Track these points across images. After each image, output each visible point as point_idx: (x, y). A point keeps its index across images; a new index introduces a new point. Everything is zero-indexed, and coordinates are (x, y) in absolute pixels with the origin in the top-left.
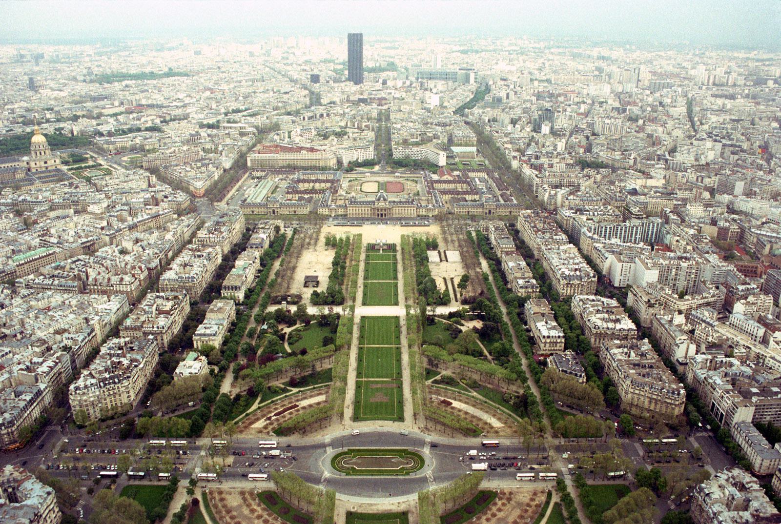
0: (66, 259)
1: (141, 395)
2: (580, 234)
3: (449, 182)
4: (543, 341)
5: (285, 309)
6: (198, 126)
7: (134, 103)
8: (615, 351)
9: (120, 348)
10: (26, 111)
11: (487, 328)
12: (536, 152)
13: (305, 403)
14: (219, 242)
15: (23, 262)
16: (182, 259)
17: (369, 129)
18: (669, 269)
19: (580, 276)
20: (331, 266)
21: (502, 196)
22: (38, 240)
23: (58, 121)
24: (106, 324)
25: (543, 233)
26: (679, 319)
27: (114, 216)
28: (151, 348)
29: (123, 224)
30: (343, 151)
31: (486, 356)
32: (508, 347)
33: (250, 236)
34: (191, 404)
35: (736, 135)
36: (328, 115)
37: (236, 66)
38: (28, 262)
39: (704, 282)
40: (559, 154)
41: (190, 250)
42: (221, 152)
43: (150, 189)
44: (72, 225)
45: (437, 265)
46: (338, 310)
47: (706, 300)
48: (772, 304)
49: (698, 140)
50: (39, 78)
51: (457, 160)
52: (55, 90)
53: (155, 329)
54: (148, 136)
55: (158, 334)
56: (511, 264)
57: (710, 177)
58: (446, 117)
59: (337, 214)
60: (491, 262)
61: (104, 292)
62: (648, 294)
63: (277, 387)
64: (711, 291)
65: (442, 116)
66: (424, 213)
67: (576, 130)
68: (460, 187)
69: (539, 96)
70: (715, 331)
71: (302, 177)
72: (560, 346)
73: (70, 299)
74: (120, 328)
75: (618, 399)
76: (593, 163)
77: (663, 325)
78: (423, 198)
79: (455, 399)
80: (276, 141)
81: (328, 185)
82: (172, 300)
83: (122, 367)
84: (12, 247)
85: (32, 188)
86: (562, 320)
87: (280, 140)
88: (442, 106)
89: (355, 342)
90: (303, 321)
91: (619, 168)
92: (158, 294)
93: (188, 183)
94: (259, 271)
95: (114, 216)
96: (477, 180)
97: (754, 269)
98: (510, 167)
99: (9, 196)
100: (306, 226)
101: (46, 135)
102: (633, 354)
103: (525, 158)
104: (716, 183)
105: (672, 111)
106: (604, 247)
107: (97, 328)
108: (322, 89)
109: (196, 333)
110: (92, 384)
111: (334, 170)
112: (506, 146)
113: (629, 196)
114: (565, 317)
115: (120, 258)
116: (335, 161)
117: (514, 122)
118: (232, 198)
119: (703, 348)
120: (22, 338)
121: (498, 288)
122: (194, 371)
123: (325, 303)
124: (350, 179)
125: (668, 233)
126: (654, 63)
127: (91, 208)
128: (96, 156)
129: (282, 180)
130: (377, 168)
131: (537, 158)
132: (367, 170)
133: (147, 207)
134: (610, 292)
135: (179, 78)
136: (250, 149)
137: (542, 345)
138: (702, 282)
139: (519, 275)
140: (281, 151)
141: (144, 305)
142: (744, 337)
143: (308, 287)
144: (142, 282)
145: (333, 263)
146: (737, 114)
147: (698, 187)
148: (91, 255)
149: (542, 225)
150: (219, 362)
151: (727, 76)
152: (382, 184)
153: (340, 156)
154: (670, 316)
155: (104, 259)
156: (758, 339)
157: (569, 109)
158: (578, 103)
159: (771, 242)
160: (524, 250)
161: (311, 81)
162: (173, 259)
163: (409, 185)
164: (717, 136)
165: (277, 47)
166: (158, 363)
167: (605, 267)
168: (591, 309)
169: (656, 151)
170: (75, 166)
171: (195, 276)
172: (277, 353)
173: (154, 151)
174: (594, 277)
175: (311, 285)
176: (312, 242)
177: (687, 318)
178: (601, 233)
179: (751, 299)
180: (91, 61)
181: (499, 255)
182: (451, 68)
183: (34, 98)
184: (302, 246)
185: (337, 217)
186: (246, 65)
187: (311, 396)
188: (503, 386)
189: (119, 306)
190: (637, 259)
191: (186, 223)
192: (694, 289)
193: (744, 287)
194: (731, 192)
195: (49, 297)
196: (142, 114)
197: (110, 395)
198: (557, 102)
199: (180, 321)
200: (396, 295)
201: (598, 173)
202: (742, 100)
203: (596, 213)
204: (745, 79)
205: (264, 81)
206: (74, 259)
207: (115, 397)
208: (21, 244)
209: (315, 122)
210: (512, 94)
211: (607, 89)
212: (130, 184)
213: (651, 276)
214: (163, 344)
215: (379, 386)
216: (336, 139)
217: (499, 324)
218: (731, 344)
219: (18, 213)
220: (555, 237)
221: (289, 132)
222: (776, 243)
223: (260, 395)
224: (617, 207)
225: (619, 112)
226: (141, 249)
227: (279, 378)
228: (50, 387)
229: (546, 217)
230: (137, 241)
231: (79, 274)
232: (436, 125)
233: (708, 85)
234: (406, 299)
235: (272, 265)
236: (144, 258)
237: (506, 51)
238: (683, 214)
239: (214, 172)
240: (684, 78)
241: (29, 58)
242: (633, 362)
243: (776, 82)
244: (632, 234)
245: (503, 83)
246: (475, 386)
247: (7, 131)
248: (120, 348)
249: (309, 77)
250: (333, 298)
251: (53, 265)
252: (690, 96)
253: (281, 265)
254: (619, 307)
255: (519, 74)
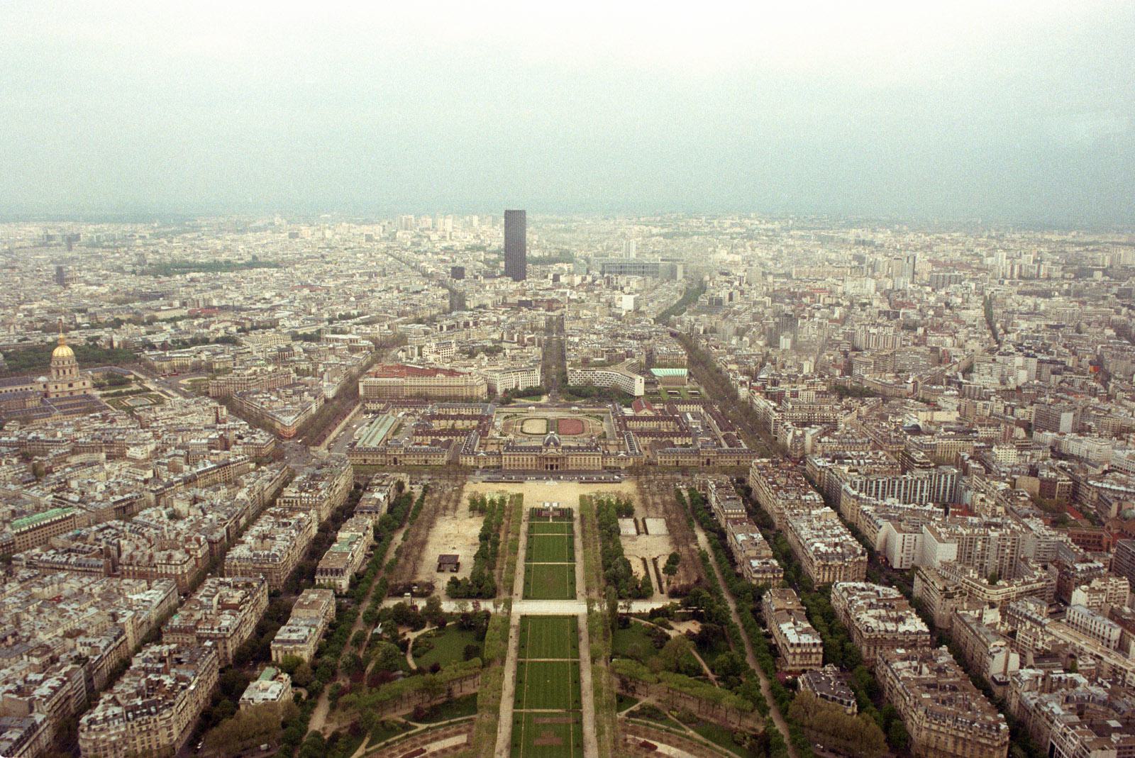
0: (90, 526)
1: (189, 732)
2: (840, 492)
3: (649, 419)
4: (791, 651)
5: (409, 604)
6: (289, 337)
7: (201, 304)
8: (899, 665)
9: (162, 660)
10: (49, 312)
11: (708, 633)
12: (773, 375)
13: (435, 747)
14: (314, 505)
15: (27, 528)
16: (260, 529)
17: (534, 344)
18: (972, 541)
19: (843, 554)
20: (477, 540)
21: (725, 438)
22: (50, 497)
23: (93, 327)
24: (142, 623)
25: (787, 491)
26: (992, 616)
27: (164, 464)
28: (208, 660)
29: (176, 475)
30: (497, 374)
31: (707, 675)
32: (739, 661)
33: (361, 496)
34: (263, 746)
35: (1058, 348)
36: (476, 324)
37: (348, 253)
38: (34, 529)
39: (1025, 560)
40: (806, 377)
41: (272, 515)
42: (322, 374)
43: (219, 426)
44: (102, 475)
45: (633, 538)
46: (486, 605)
47: (1029, 586)
48: (1128, 591)
49: (1003, 355)
50: (70, 267)
51: (660, 387)
52: (91, 285)
53: (216, 632)
54: (218, 350)
55: (220, 639)
56: (741, 537)
57: (1023, 407)
58: (643, 327)
59: (487, 464)
60: (712, 534)
61: (142, 576)
62: (943, 578)
63: (395, 722)
64: (1036, 573)
65: (637, 325)
66: (613, 464)
67: (830, 343)
68: (665, 426)
69: (775, 296)
70: (1047, 632)
71: (437, 412)
72: (817, 659)
73: (92, 586)
74: (164, 629)
75: (907, 738)
76: (855, 389)
77: (967, 625)
78: (612, 442)
79: (662, 741)
80: (401, 360)
81: (475, 423)
82: (243, 589)
83: (164, 689)
84: (12, 507)
85: (49, 421)
86: (818, 619)
87: (407, 358)
88: (637, 311)
89: (512, 654)
90: (434, 623)
91: (893, 397)
92: (221, 579)
93: (273, 418)
94: (372, 547)
95: (164, 464)
96: (689, 415)
97: (1097, 540)
98: (736, 396)
99: (14, 432)
100: (443, 482)
101: (73, 347)
102: (925, 670)
103: (758, 384)
104: (1033, 415)
105: (964, 314)
106: (876, 511)
107: (129, 628)
108: (468, 288)
109: (276, 638)
110: (115, 715)
111: (483, 402)
112: (730, 367)
113: (909, 437)
114: (823, 615)
115: (169, 525)
116: (485, 389)
117: (740, 333)
118: (335, 441)
119: (1030, 657)
120: (15, 643)
121: (723, 574)
122: (270, 696)
123: (469, 596)
124: (505, 415)
125: (968, 488)
126: (935, 249)
127: (131, 452)
128: (142, 377)
129: (408, 415)
130: (544, 399)
131: (775, 383)
132: (532, 402)
133: (214, 451)
134: (888, 577)
135: (266, 269)
136: (364, 371)
137: (790, 658)
138: (1022, 560)
139: (753, 553)
140: (408, 375)
141: (200, 595)
142: (1090, 641)
143: (443, 571)
144: (200, 562)
145: (480, 536)
146: (1055, 318)
147: (1007, 422)
148: (126, 520)
149: (784, 480)
150: (307, 684)
151: (1036, 265)
152: (552, 421)
153: (492, 382)
154: (978, 612)
155: (146, 526)
156: (1112, 644)
157: (818, 314)
158: (831, 305)
159: (1118, 499)
160: (759, 516)
161: (453, 277)
162: (246, 527)
163: (592, 424)
164: (1030, 348)
165: (406, 229)
166: (216, 683)
167: (878, 540)
168: (860, 603)
169: (944, 371)
170: (112, 391)
171: (278, 554)
172: (396, 670)
173: (226, 371)
174: (863, 554)
175: (448, 569)
176: (451, 505)
177: (1003, 613)
178: (871, 491)
179: (1096, 583)
180: (145, 245)
181: (723, 525)
182: (649, 258)
183: (62, 295)
184: (436, 511)
185: (486, 469)
186: (360, 252)
187: (446, 736)
188: (733, 720)
189: (163, 596)
190: (924, 527)
191: (268, 475)
192: (1010, 570)
193: (1084, 566)
194: (1054, 427)
195: (60, 581)
196: (212, 319)
197: (141, 732)
198: (800, 305)
199: (253, 620)
200: (573, 583)
201: (863, 404)
202: (1061, 299)
203: (862, 461)
204: (1062, 270)
205: (385, 275)
206: (101, 526)
207: (149, 735)
208: (26, 503)
209: (457, 334)
210: (736, 293)
211: (871, 285)
212: (189, 419)
213: (947, 552)
214: (226, 654)
215: (547, 720)
216: (486, 358)
217: (725, 627)
218: (1072, 652)
219: (26, 458)
220: (803, 497)
221: (420, 348)
222: (1127, 500)
223: (369, 734)
224: (892, 453)
225: (888, 318)
226: (200, 513)
227: (397, 708)
228: (51, 719)
229: (790, 469)
230: (195, 500)
231: (107, 548)
232: (629, 338)
233: (1012, 278)
234: (588, 589)
235: (392, 538)
236: (204, 526)
237: (727, 234)
238: (988, 461)
239: (310, 403)
240: (979, 269)
241: (59, 240)
242: (926, 682)
243: (1105, 272)
244: (915, 491)
245: (724, 278)
246: (690, 720)
247: (20, 341)
248: (162, 660)
249: (450, 270)
250: (480, 587)
251: (71, 534)
252: (987, 293)
253: (404, 539)
254: (901, 599)
255: (746, 266)
